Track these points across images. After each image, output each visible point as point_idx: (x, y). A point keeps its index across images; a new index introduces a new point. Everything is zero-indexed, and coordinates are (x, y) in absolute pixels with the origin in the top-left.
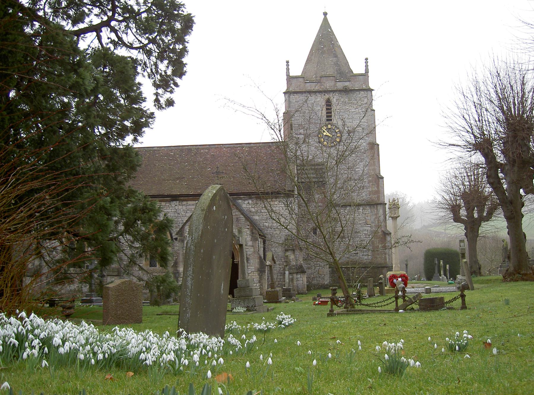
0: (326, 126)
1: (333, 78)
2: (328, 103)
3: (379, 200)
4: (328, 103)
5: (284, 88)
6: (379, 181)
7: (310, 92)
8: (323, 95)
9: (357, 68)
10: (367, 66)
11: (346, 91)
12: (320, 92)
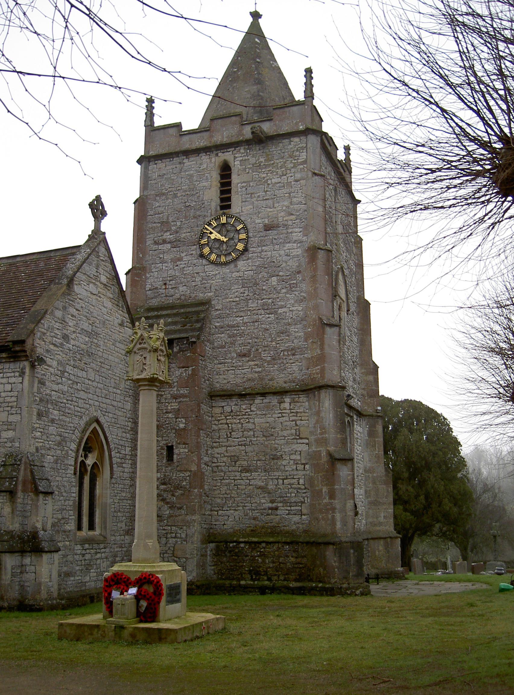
0: (217, 219)
1: (238, 118)
2: (226, 171)
3: (323, 377)
4: (226, 171)
6: (324, 333)
7: (187, 153)
8: (213, 155)
11: (259, 140)
12: (206, 150)
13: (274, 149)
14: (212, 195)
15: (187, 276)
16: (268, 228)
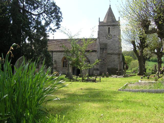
2: (109, 28)
4: (109, 28)
5: (98, 24)
9: (117, 20)
10: (119, 19)
13: (115, 27)
14: (108, 31)
15: (104, 40)
16: (114, 36)
